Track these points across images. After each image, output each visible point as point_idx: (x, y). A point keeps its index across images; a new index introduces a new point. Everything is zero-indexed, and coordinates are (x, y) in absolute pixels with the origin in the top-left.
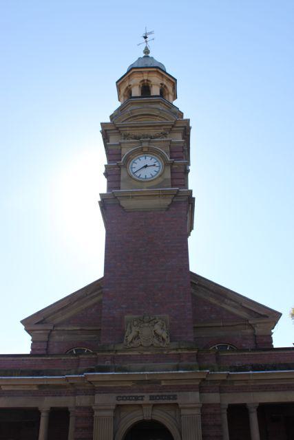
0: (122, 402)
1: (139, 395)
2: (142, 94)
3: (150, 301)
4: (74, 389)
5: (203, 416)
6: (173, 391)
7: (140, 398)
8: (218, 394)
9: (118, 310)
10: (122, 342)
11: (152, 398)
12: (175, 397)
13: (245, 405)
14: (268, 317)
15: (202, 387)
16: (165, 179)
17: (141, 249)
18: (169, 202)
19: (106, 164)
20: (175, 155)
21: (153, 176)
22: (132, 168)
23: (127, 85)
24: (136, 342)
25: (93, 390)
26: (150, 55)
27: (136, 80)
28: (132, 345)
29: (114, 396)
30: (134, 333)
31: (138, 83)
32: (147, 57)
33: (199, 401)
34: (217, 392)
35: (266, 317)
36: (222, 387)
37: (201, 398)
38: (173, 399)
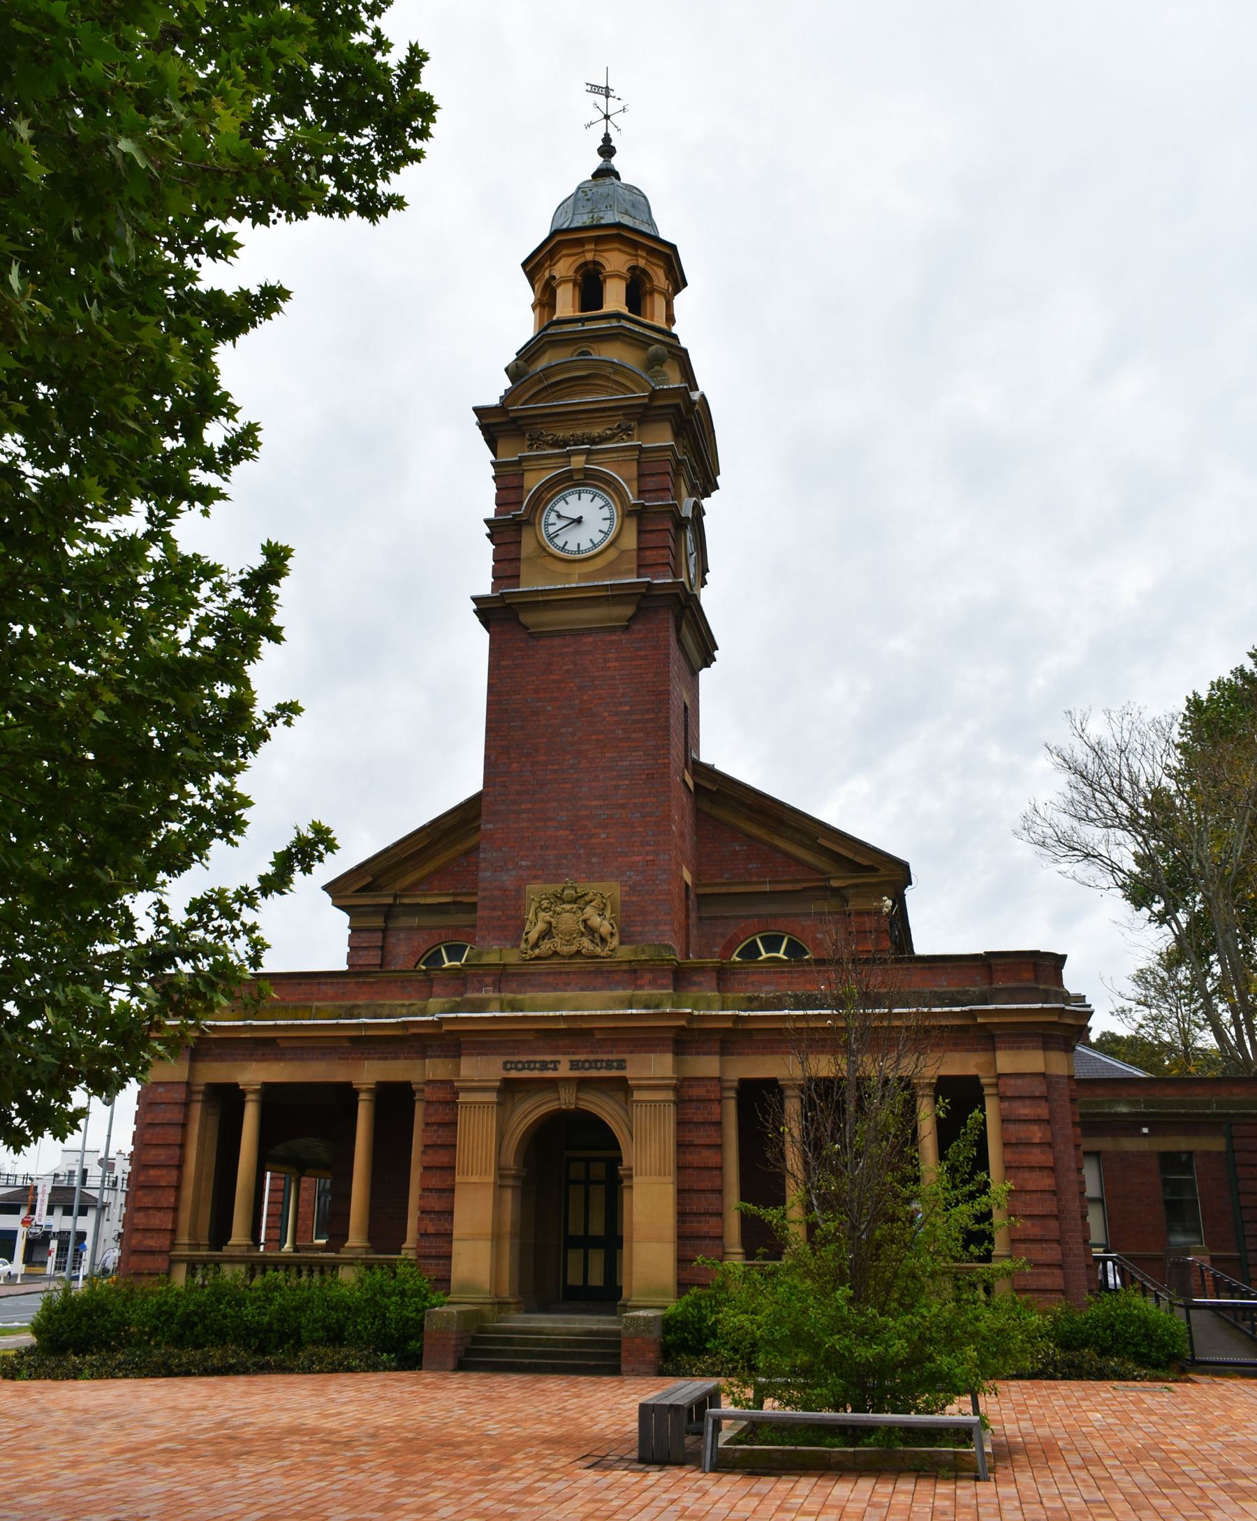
0: (513, 1074)
1: (548, 1058)
2: (572, 1287)
3: (582, 852)
5: (680, 1103)
6: (618, 1052)
8: (717, 1058)
9: (513, 873)
10: (518, 946)
11: (574, 1065)
12: (621, 1065)
14: (877, 870)
15: (685, 1038)
16: (623, 552)
17: (563, 730)
18: (629, 611)
19: (491, 515)
20: (651, 483)
22: (547, 525)
23: (547, 275)
24: (546, 946)
25: (451, 1042)
27: (564, 267)
29: (498, 1061)
30: (541, 926)
31: (571, 273)
32: (606, 173)
33: (669, 1073)
34: (715, 1053)
35: (871, 869)
36: (732, 1038)
37: (677, 1066)
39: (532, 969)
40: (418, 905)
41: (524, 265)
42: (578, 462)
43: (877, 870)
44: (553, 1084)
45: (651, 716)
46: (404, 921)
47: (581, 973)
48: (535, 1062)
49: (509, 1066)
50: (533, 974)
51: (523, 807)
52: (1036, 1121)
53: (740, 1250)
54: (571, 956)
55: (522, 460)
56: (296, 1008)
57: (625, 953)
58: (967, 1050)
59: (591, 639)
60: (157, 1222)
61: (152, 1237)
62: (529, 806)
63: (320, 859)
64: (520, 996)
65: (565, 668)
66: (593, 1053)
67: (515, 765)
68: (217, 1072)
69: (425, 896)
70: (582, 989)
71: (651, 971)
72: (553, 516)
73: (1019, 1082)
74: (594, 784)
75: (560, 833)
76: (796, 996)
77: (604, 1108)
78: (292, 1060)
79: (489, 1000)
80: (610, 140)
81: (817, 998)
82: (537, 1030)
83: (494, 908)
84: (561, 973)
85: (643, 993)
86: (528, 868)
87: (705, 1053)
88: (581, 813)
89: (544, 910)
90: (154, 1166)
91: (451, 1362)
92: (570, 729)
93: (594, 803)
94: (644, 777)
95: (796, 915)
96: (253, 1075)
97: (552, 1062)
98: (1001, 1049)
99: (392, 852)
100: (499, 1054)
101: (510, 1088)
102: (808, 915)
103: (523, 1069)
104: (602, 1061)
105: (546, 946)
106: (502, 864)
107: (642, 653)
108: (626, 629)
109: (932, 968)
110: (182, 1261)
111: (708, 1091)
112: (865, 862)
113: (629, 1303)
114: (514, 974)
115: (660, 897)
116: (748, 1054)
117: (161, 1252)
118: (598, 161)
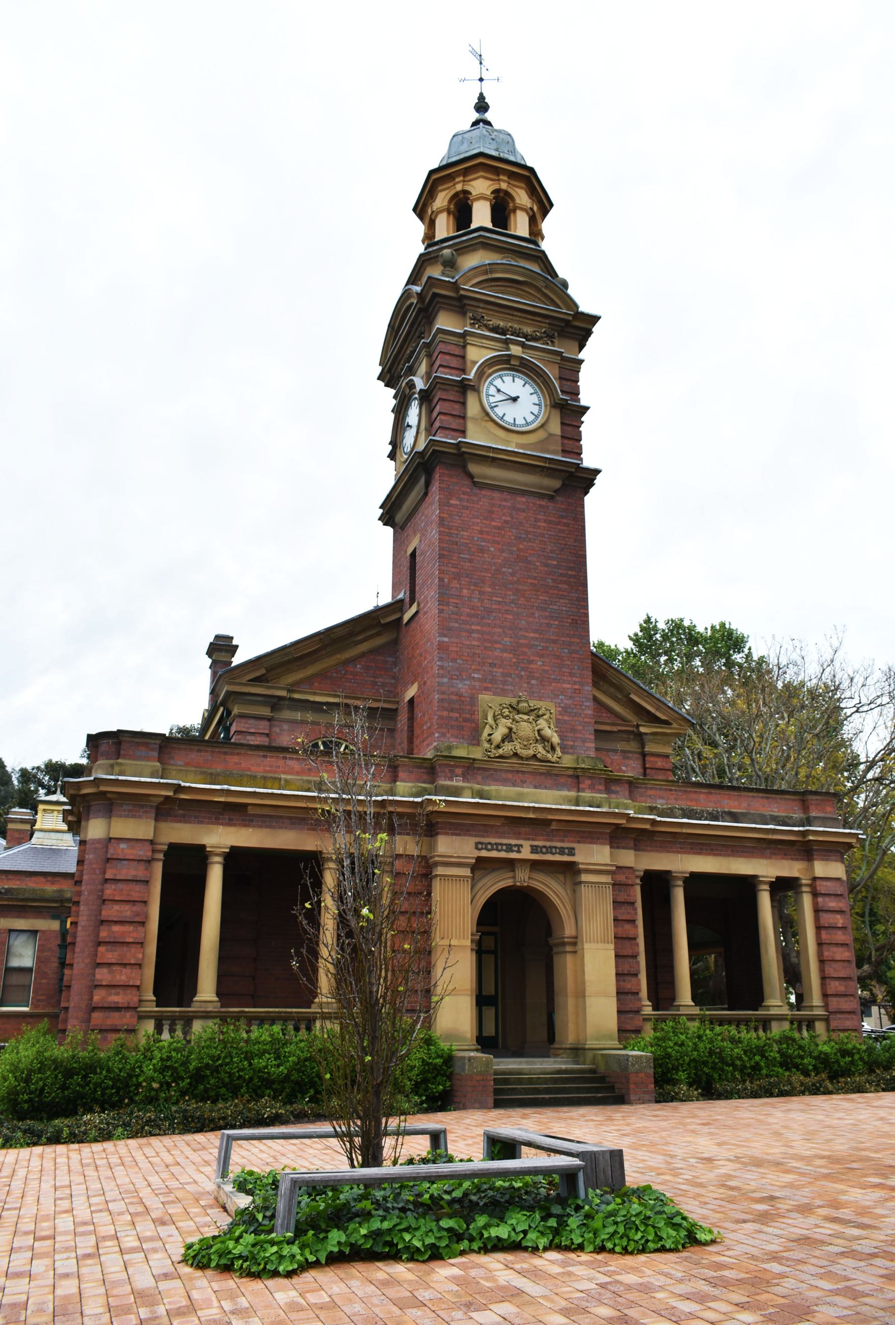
0: (484, 854)
3: (523, 673)
4: (391, 819)
7: (516, 849)
9: (468, 682)
11: (534, 849)
13: (668, 872)
14: (670, 724)
15: (620, 834)
16: (551, 435)
17: (504, 570)
18: (556, 484)
21: (515, 424)
22: (527, 424)
24: (507, 748)
25: (429, 824)
26: (488, 116)
28: (501, 751)
29: (472, 841)
31: (489, 193)
34: (630, 848)
38: (568, 855)
39: (496, 766)
40: (308, 701)
41: (415, 210)
42: (516, 350)
43: (670, 724)
44: (511, 864)
45: (573, 573)
46: (287, 714)
47: (535, 773)
48: (502, 844)
49: (480, 846)
50: (495, 770)
51: (473, 627)
52: (840, 912)
53: (154, 998)
54: (527, 759)
55: (464, 335)
56: (264, 778)
57: (568, 761)
58: (792, 859)
59: (524, 500)
60: (123, 978)
61: (118, 994)
62: (479, 628)
63: (713, 627)
64: (486, 788)
65: (504, 518)
66: (548, 840)
67: (465, 591)
68: (183, 833)
69: (315, 694)
70: (535, 787)
71: (590, 778)
72: (492, 391)
73: (828, 883)
74: (530, 619)
75: (505, 655)
76: (682, 809)
77: (552, 888)
78: (261, 827)
79: (463, 788)
80: (484, 98)
81: (696, 813)
82: (506, 817)
83: (452, 710)
84: (518, 772)
85: (587, 795)
86: (479, 680)
87: (623, 848)
88: (522, 641)
89: (505, 717)
90: (116, 922)
91: (491, 1101)
92: (510, 570)
93: (532, 635)
94: (569, 621)
95: (608, 750)
96: (220, 838)
97: (516, 845)
98: (817, 859)
99: (287, 650)
100: (472, 835)
101: (481, 866)
102: (615, 751)
103: (502, 850)
104: (556, 848)
105: (507, 748)
106: (457, 673)
107: (565, 521)
108: (551, 498)
109: (767, 798)
110: (150, 1017)
111: (626, 878)
112: (663, 717)
113: (587, 1046)
114: (479, 769)
115: (586, 720)
116: (650, 851)
117: (128, 1008)
118: (475, 116)
